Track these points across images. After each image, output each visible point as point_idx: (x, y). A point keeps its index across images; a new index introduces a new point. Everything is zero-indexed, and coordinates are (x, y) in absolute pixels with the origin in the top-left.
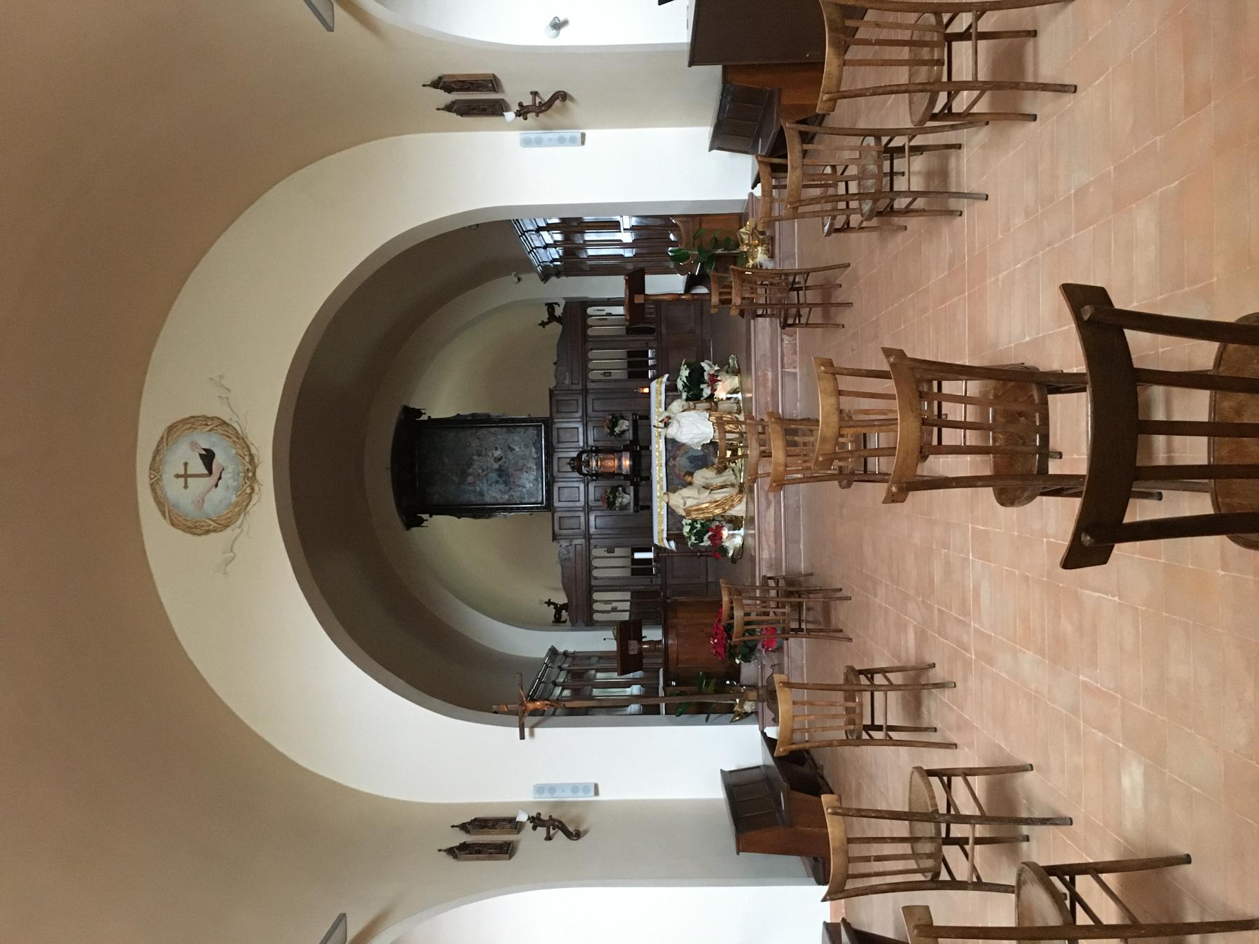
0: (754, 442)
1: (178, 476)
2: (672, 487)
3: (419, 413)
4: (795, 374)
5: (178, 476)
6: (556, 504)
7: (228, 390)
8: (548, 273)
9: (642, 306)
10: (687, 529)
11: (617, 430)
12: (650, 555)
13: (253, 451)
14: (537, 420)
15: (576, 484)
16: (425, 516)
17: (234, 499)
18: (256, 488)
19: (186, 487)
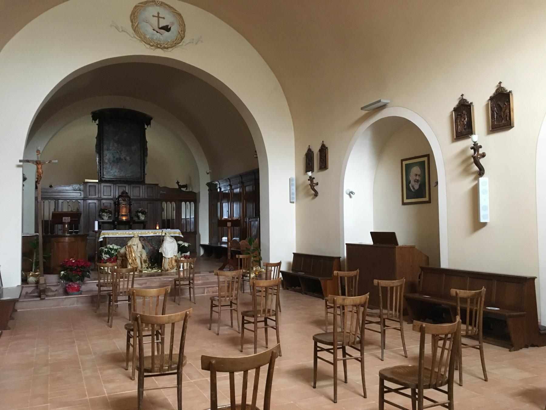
0: (234, 274)
1: (158, 13)
2: (141, 238)
3: (149, 124)
4: (204, 293)
5: (158, 13)
6: (103, 184)
7: (196, 43)
8: (212, 187)
9: (226, 225)
10: (111, 247)
11: (140, 214)
12: (96, 229)
13: (170, 49)
14: (144, 177)
15: (112, 195)
16: (97, 122)
17: (148, 37)
18: (153, 48)
19: (154, 16)
